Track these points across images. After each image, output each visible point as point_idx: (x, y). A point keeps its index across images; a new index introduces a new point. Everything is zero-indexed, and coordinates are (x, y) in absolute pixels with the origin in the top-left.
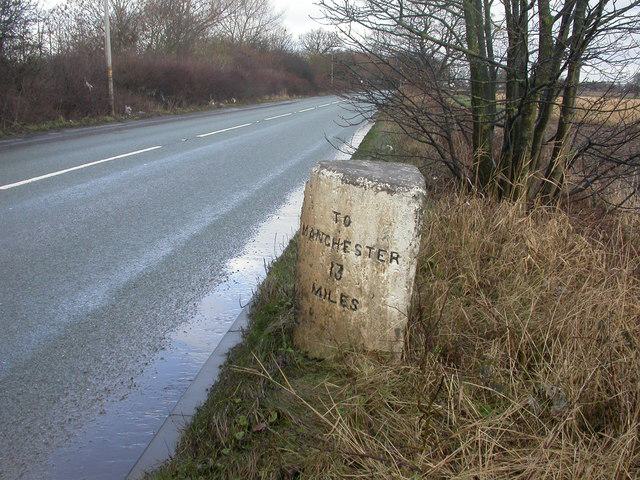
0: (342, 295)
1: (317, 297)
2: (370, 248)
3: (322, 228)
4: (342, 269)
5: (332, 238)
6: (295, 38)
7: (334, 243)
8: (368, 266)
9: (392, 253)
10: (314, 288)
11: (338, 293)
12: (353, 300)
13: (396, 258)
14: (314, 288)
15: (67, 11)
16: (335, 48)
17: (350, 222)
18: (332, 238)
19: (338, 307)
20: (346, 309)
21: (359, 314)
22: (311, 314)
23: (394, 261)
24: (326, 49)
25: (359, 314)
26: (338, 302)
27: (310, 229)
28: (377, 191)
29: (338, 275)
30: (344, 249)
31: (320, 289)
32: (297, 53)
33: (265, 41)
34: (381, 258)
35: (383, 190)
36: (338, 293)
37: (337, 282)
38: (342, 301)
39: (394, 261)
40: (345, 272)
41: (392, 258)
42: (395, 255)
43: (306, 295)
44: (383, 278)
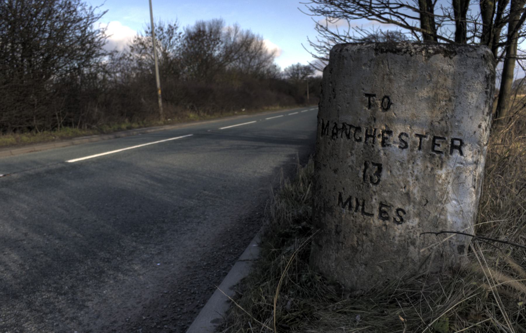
0: (381, 205)
1: (346, 211)
2: (421, 136)
3: (349, 119)
4: (380, 169)
5: (364, 130)
6: (282, 70)
7: (367, 136)
8: (419, 162)
9: (453, 140)
10: (340, 199)
11: (375, 201)
12: (398, 210)
13: (459, 148)
14: (340, 199)
15: (131, 58)
16: (309, 76)
17: (390, 104)
18: (364, 130)
19: (376, 221)
20: (387, 223)
21: (407, 227)
22: (338, 233)
23: (456, 153)
24: (303, 77)
25: (407, 227)
26: (376, 213)
27: (331, 125)
28: (429, 55)
29: (376, 178)
30: (383, 144)
31: (350, 199)
32: (284, 80)
33: (263, 73)
34: (437, 148)
35: (437, 52)
36: (375, 201)
37: (374, 188)
38: (381, 212)
39: (456, 153)
40: (385, 174)
41: (453, 147)
42: (457, 143)
43: (330, 210)
44: (440, 176)
